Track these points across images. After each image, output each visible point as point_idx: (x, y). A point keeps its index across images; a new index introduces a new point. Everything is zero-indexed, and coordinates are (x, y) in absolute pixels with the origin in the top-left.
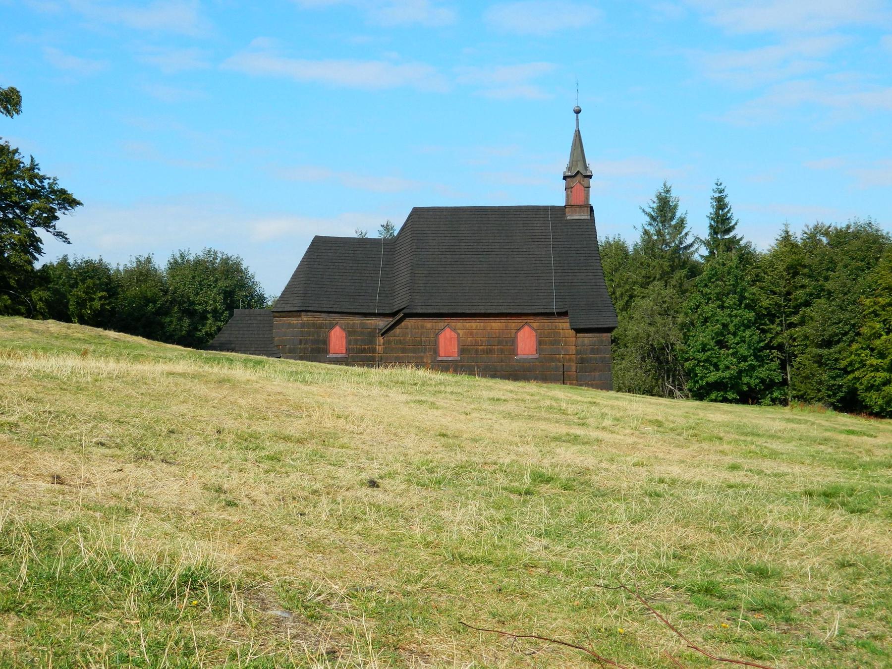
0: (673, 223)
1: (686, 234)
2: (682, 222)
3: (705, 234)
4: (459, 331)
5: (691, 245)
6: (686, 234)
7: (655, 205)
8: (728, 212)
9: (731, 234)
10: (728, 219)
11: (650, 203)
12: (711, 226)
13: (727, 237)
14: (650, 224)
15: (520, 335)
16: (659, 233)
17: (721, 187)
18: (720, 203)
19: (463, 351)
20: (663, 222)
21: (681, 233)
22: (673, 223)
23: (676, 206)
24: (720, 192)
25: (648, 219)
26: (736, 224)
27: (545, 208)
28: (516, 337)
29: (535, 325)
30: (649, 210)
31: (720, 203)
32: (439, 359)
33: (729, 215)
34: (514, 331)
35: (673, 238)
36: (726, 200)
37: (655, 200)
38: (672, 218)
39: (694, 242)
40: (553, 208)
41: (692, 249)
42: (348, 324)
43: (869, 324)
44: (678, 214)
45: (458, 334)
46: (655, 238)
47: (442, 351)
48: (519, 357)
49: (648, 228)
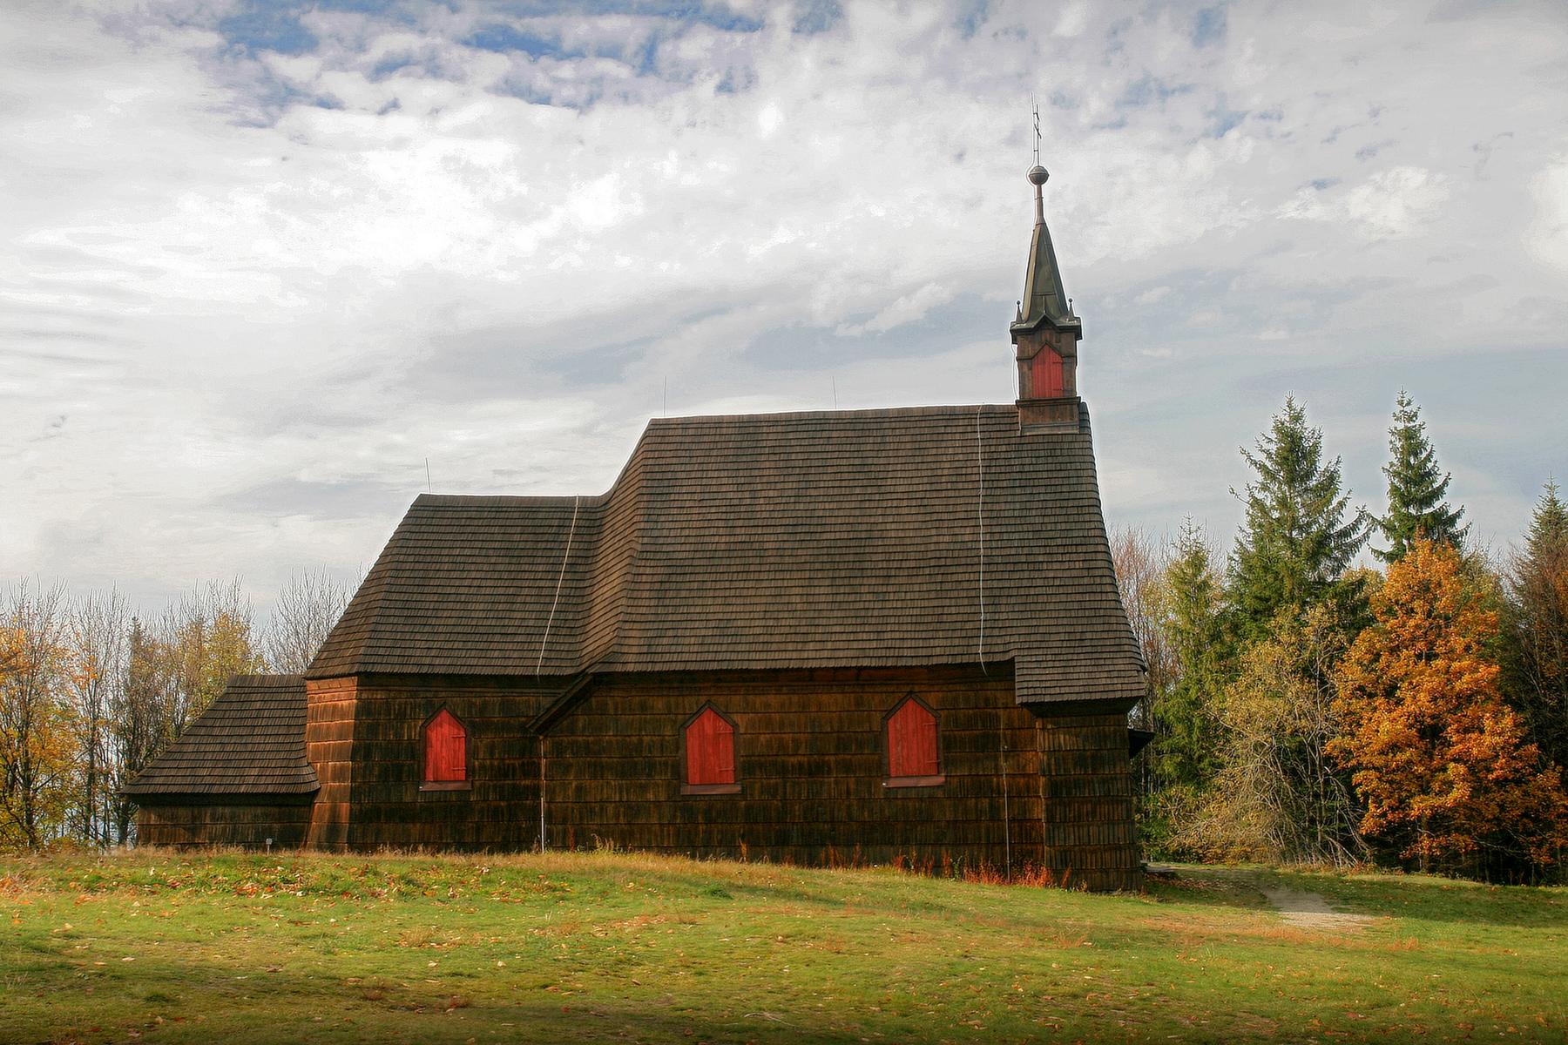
0: (1313, 483)
1: (1341, 504)
2: (1331, 480)
3: (1383, 507)
4: (736, 718)
5: (1354, 527)
6: (1341, 504)
7: (1273, 448)
8: (1428, 458)
9: (1437, 505)
10: (1429, 474)
11: (1263, 441)
12: (1395, 490)
13: (1426, 511)
14: (1265, 488)
15: (895, 725)
16: (1283, 503)
17: (1412, 408)
18: (1411, 442)
19: (747, 768)
20: (1291, 481)
21: (1329, 502)
22: (1313, 483)
23: (1315, 450)
24: (1410, 419)
25: (1260, 477)
26: (1445, 483)
27: (968, 413)
28: (884, 730)
29: (933, 699)
30: (1261, 457)
31: (1411, 442)
32: (687, 790)
33: (1430, 465)
34: (877, 716)
35: (1314, 510)
36: (1423, 435)
37: (1274, 436)
38: (1308, 475)
39: (1358, 521)
40: (989, 412)
41: (1354, 537)
42: (471, 705)
43: (1164, 746)
44: (1321, 465)
45: (735, 726)
46: (1276, 515)
47: (693, 772)
48: (893, 783)
49: (1260, 496)
